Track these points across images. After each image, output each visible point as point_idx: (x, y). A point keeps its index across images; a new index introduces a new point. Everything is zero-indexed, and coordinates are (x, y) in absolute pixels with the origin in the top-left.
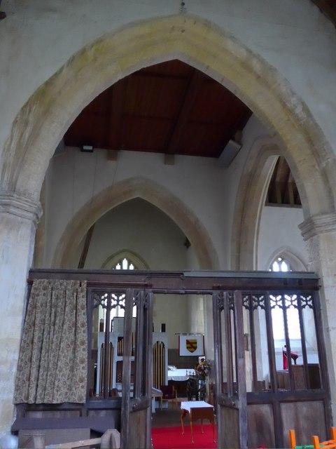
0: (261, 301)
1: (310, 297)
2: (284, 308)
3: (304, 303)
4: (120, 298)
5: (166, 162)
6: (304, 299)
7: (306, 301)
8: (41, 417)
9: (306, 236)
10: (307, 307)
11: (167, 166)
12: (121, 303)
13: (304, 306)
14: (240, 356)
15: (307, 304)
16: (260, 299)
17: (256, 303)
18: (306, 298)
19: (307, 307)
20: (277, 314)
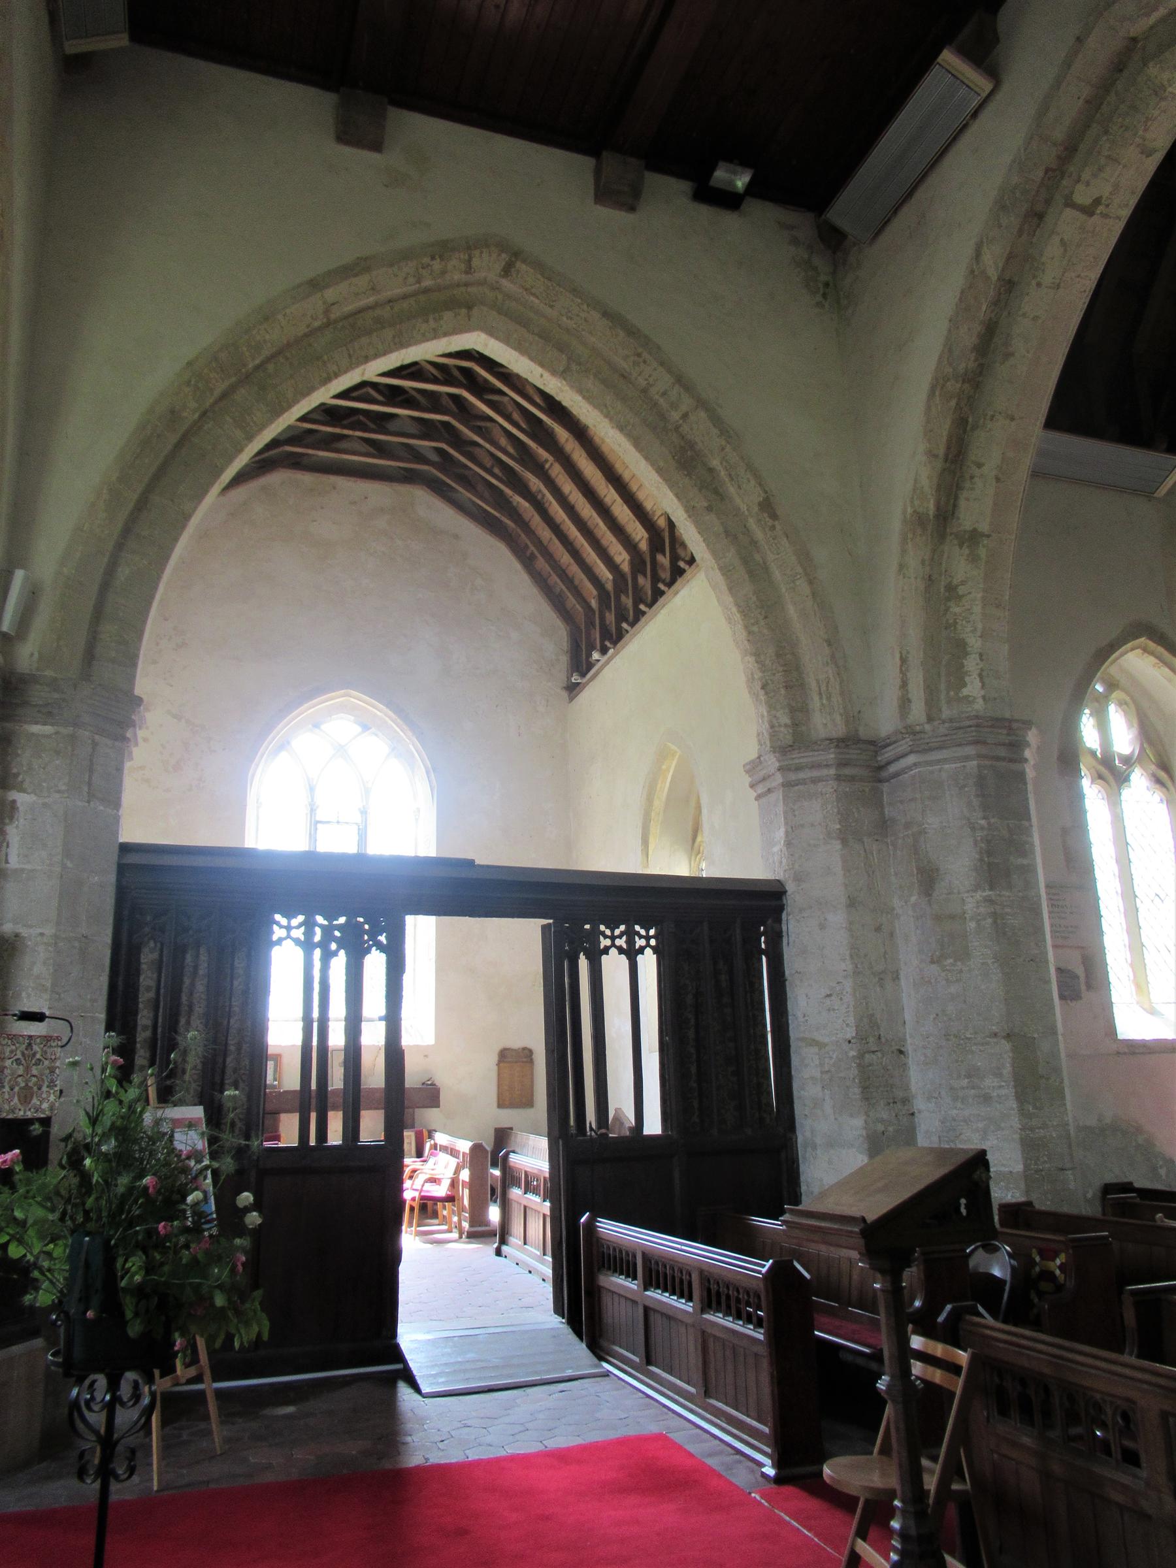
0: (620, 937)
1: (301, 918)
2: (632, 954)
3: (640, 943)
4: (617, 932)
5: (604, 194)
6: (608, 932)
7: (613, 938)
8: (259, 1221)
9: (761, 789)
10: (613, 951)
11: (598, 207)
12: (618, 942)
13: (641, 950)
14: (753, 955)
15: (613, 945)
16: (617, 932)
17: (608, 942)
18: (289, 920)
19: (613, 951)
20: (614, 966)
